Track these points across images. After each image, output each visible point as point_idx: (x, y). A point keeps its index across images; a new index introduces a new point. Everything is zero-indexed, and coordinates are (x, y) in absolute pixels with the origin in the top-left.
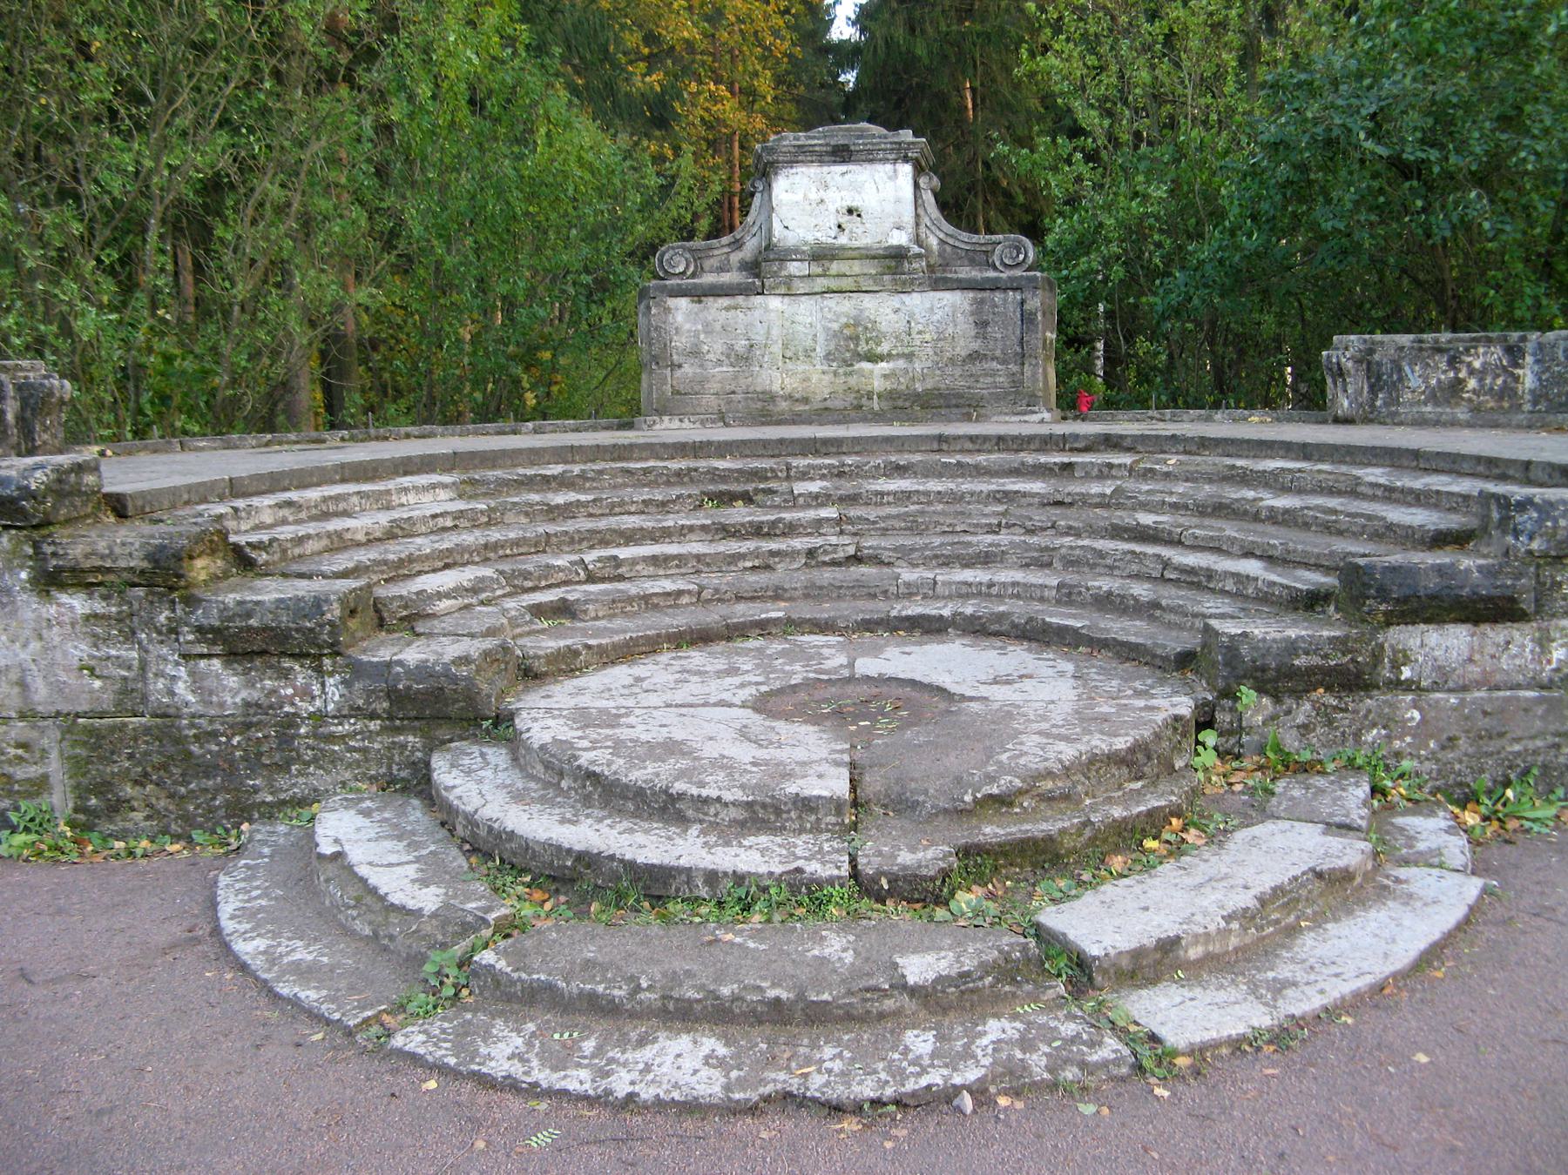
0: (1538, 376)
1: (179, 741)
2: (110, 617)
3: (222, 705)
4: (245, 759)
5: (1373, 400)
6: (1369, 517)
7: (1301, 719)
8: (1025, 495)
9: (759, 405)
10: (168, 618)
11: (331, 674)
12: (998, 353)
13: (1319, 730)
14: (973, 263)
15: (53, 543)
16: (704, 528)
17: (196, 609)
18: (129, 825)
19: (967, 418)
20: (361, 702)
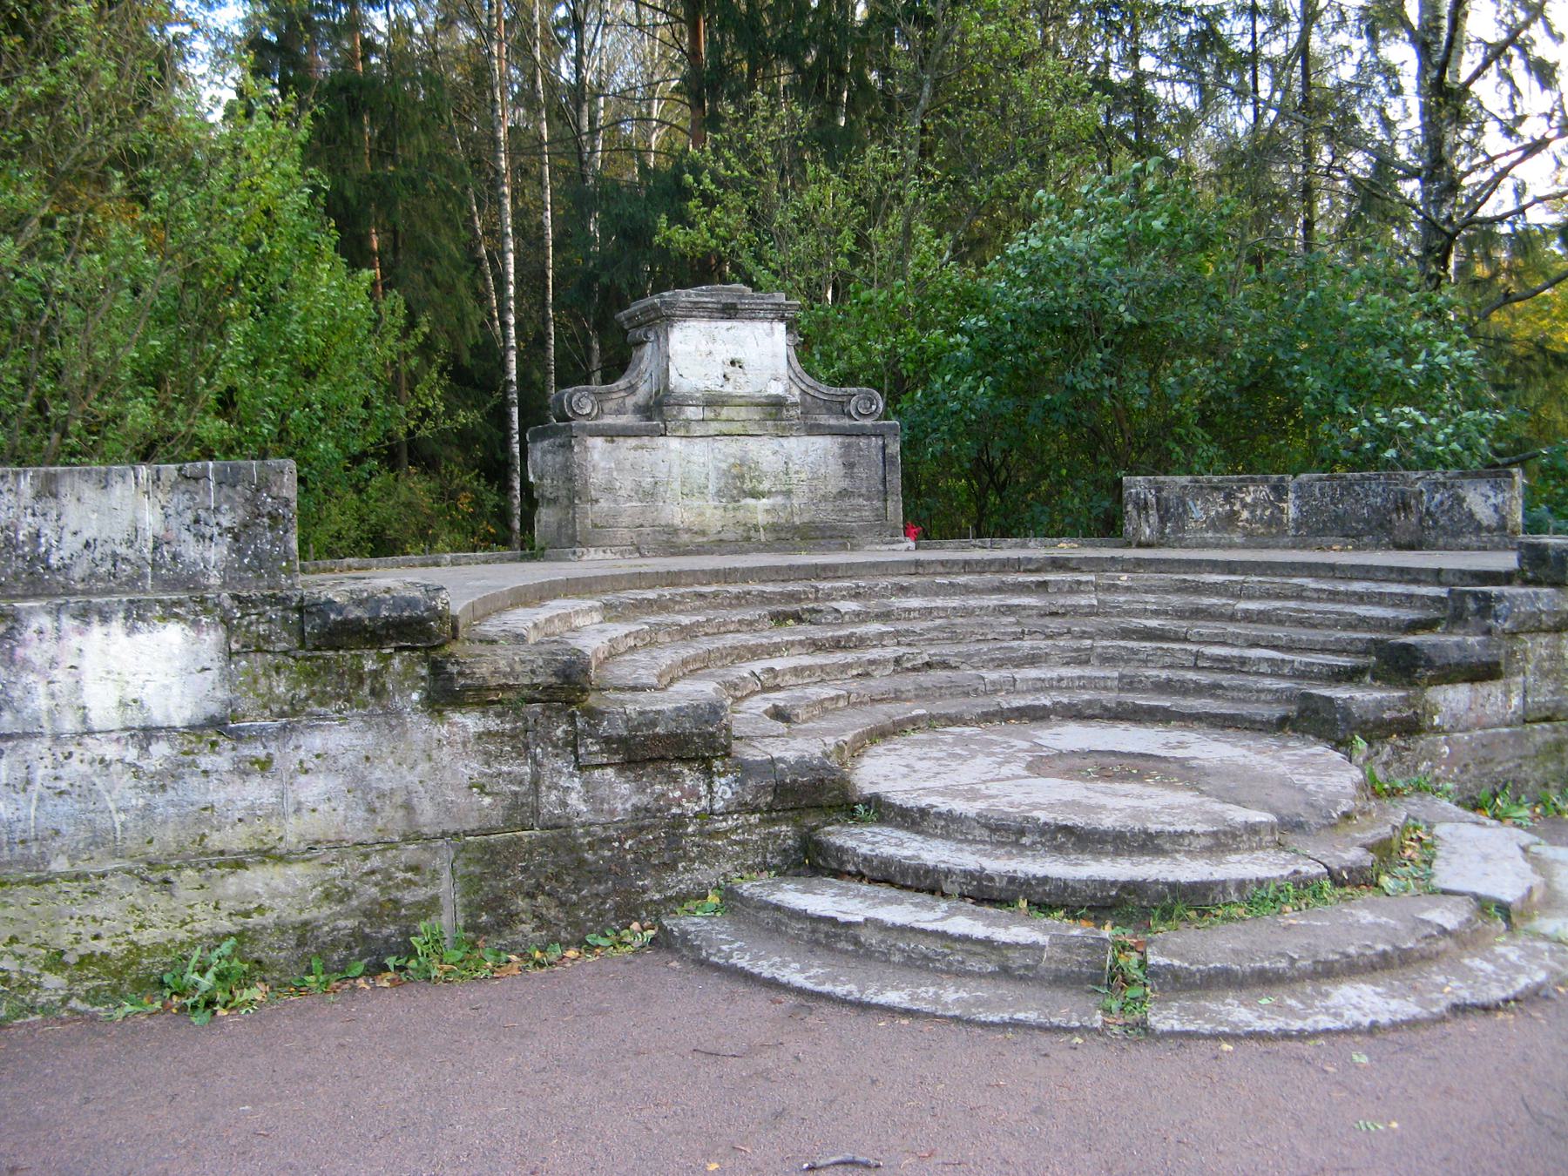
0: (1299, 508)
1: (574, 849)
2: (503, 734)
3: (612, 812)
4: (634, 861)
5: (1163, 529)
6: (1338, 613)
7: (1384, 758)
8: (1025, 608)
9: (665, 537)
10: (566, 732)
11: (720, 775)
12: (863, 491)
13: (1395, 765)
14: (830, 411)
15: (457, 663)
16: (801, 643)
17: (601, 721)
18: (518, 938)
19: (843, 547)
20: (749, 798)
